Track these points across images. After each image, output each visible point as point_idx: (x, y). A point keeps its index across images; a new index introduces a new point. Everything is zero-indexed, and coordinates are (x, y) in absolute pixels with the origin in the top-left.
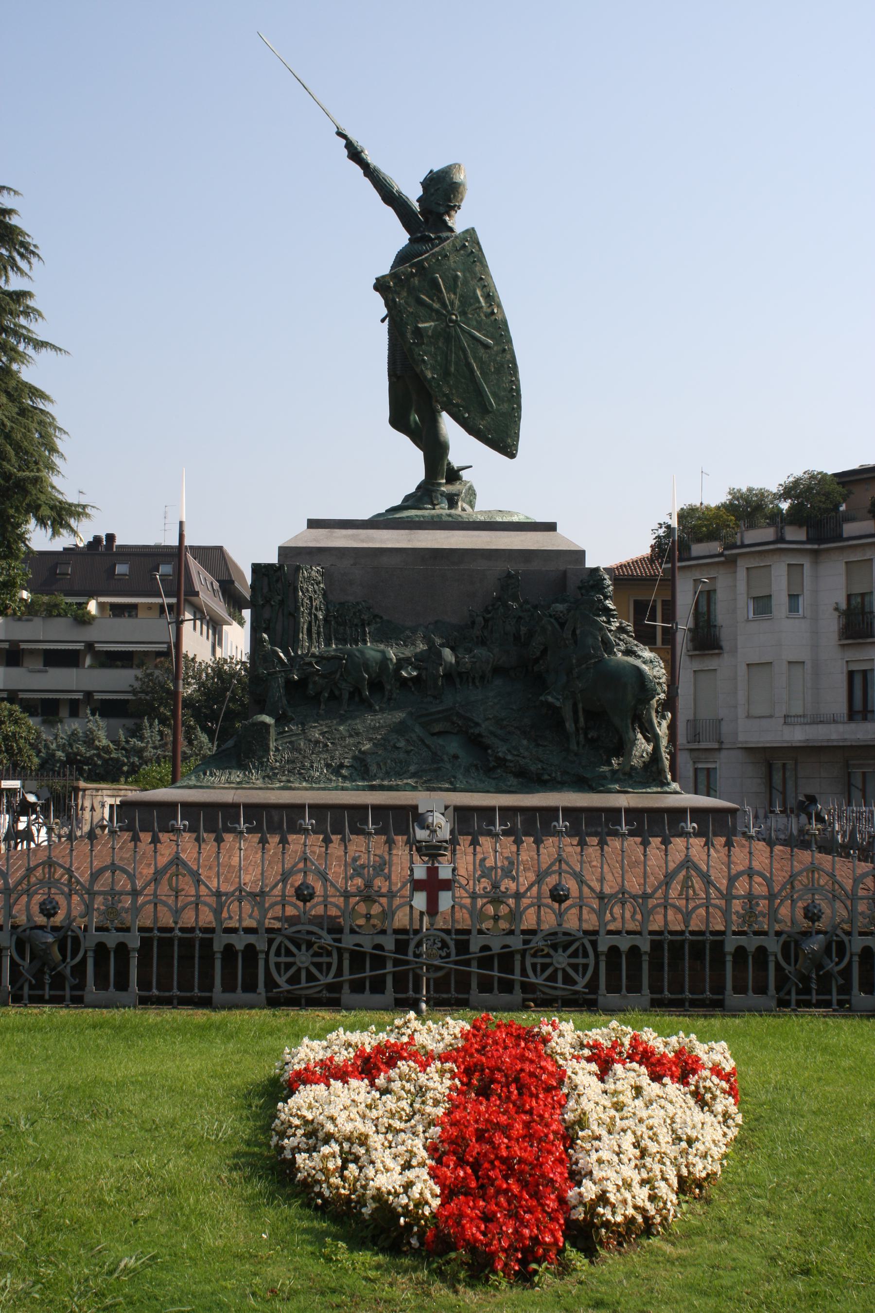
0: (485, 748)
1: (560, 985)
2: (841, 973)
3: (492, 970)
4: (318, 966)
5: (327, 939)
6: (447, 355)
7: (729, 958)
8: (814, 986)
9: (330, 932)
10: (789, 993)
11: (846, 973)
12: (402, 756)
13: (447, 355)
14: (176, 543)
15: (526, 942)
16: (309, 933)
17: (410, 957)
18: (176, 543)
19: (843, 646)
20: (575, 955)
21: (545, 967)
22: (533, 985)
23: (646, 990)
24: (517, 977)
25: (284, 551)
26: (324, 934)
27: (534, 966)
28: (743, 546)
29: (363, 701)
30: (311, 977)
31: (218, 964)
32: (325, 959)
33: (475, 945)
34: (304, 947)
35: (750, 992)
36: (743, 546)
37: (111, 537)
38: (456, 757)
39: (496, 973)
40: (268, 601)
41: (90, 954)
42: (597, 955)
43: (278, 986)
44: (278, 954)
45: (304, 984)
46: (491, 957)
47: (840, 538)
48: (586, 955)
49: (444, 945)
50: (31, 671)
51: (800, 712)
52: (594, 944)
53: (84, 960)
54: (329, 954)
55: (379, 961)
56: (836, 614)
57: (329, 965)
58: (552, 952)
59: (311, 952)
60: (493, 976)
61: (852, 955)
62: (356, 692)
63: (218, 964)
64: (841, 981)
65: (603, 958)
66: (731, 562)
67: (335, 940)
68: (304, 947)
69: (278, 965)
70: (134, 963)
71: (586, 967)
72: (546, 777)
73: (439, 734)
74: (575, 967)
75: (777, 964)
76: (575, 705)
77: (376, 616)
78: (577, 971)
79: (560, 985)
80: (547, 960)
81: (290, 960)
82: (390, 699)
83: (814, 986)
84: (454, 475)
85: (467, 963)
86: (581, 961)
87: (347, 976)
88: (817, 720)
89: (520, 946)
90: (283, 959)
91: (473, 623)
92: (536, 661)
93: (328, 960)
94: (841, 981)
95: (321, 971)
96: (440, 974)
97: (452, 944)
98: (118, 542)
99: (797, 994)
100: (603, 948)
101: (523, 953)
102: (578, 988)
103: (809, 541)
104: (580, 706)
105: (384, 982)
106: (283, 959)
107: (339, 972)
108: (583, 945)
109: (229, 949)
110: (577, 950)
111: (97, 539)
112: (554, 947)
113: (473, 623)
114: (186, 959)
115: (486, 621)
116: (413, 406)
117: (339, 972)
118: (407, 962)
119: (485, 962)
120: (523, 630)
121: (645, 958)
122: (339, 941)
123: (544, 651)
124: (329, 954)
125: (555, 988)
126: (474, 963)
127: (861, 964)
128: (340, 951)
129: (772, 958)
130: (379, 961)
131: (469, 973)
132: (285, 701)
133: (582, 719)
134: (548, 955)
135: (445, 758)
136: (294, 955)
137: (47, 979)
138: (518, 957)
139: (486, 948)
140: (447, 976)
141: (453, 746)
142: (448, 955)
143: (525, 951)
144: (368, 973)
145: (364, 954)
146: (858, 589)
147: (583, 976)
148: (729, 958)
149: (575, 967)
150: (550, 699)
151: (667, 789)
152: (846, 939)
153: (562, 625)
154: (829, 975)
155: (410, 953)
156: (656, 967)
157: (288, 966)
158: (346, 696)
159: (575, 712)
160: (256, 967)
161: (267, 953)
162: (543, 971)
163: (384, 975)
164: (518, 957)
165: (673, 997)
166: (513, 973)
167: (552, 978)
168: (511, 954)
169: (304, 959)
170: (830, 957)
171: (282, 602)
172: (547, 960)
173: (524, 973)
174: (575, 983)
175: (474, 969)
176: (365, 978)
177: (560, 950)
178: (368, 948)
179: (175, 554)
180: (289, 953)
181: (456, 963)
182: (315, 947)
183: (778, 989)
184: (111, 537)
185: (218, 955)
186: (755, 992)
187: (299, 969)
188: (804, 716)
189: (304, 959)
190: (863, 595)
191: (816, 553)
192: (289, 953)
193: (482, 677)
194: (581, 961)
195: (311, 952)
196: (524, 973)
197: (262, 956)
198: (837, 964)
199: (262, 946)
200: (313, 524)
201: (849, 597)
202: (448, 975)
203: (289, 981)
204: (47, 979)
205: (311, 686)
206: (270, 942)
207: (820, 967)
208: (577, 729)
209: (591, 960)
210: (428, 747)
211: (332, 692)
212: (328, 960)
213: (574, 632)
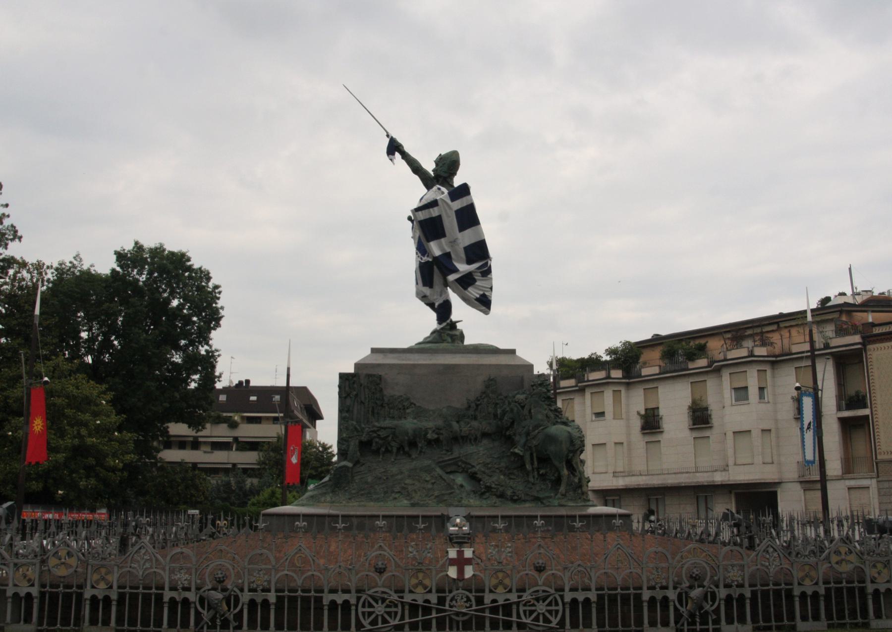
0: (479, 480)
1: (541, 623)
2: (713, 611)
3: (498, 615)
4: (389, 613)
5: (394, 597)
6: (450, 248)
7: (645, 604)
8: (698, 620)
9: (396, 592)
10: (683, 625)
11: (717, 611)
12: (430, 486)
13: (450, 248)
14: (285, 385)
15: (519, 597)
16: (383, 592)
17: (447, 607)
18: (285, 385)
19: (644, 434)
20: (550, 604)
21: (531, 612)
22: (525, 624)
23: (594, 626)
24: (514, 619)
25: (357, 366)
26: (392, 593)
27: (525, 612)
28: (588, 381)
29: (405, 453)
30: (385, 621)
31: (326, 613)
32: (393, 609)
33: (488, 598)
34: (380, 602)
35: (659, 625)
36: (588, 381)
37: (248, 382)
38: (462, 486)
39: (501, 617)
40: (348, 395)
41: (246, 607)
42: (564, 604)
43: (364, 627)
44: (363, 606)
45: (380, 625)
46: (498, 606)
47: (640, 376)
48: (557, 604)
49: (468, 600)
50: (205, 452)
51: (622, 470)
52: (562, 597)
53: (241, 611)
54: (396, 606)
55: (427, 610)
56: (639, 417)
57: (396, 613)
58: (536, 603)
59: (385, 605)
60: (498, 619)
61: (720, 600)
62: (401, 448)
63: (326, 613)
64: (714, 617)
65: (567, 606)
66: (582, 390)
67: (399, 597)
68: (380, 602)
69: (363, 613)
70: (114, 609)
71: (557, 612)
72: (516, 498)
73: (451, 473)
74: (550, 612)
75: (676, 609)
76: (532, 454)
77: (412, 403)
78: (551, 615)
79: (541, 623)
80: (533, 608)
81: (388, 610)
82: (421, 452)
83: (698, 620)
84: (453, 325)
85: (483, 610)
86: (553, 608)
87: (407, 620)
88: (631, 474)
89: (516, 600)
90: (367, 609)
91: (470, 407)
92: (507, 429)
93: (395, 609)
94: (714, 617)
95: (391, 617)
96: (465, 618)
97: (473, 599)
98: (252, 384)
99: (688, 625)
100: (568, 599)
101: (518, 604)
102: (553, 625)
103: (624, 378)
104: (535, 455)
105: (431, 623)
106: (367, 609)
107: (402, 618)
108: (555, 598)
109: (803, 595)
110: (551, 601)
111: (241, 383)
112: (537, 600)
113: (470, 407)
114: (306, 610)
115: (477, 406)
116: (432, 273)
117: (402, 618)
118: (445, 611)
119: (494, 610)
120: (499, 411)
121: (594, 605)
122: (402, 597)
123: (513, 423)
124: (396, 606)
125: (538, 626)
126: (487, 611)
127: (726, 606)
128: (402, 603)
129: (671, 604)
130: (427, 610)
131: (484, 617)
132: (358, 453)
133: (536, 463)
134: (533, 605)
135: (455, 487)
136: (373, 607)
137: (218, 622)
138: (514, 607)
139: (494, 601)
140: (471, 619)
141: (460, 479)
142: (471, 606)
143: (519, 602)
144: (420, 618)
145: (417, 606)
146: (651, 406)
147: (556, 617)
148: (645, 604)
149: (550, 612)
150: (516, 451)
151: (588, 503)
152: (716, 590)
153: (523, 407)
154: (707, 612)
155: (447, 605)
156: (601, 610)
157: (370, 614)
158: (395, 450)
159: (532, 459)
160: (350, 614)
161: (357, 606)
162: (530, 615)
163: (431, 619)
164: (514, 607)
165: (612, 629)
166: (511, 617)
167: (537, 619)
168: (511, 605)
169: (541, 607)
170: (707, 602)
171: (356, 395)
172: (533, 608)
173: (519, 616)
174: (550, 622)
175: (487, 614)
176: (418, 622)
177: (541, 602)
178: (420, 602)
179: (286, 391)
180: (371, 606)
181: (476, 611)
182: (387, 602)
183: (676, 623)
184: (248, 382)
185: (326, 607)
186: (662, 626)
187: (382, 616)
188: (623, 472)
189: (541, 607)
190: (653, 409)
191: (628, 384)
192: (371, 606)
193: (476, 439)
194: (553, 608)
195: (385, 605)
196: (519, 616)
197: (353, 608)
198: (712, 606)
199: (353, 601)
200: (374, 351)
201: (646, 410)
202: (471, 619)
203: (371, 624)
204: (218, 622)
205: (374, 444)
206: (358, 599)
207: (701, 608)
208: (533, 469)
209: (560, 608)
210: (444, 480)
211: (387, 448)
212: (395, 609)
213: (530, 411)
